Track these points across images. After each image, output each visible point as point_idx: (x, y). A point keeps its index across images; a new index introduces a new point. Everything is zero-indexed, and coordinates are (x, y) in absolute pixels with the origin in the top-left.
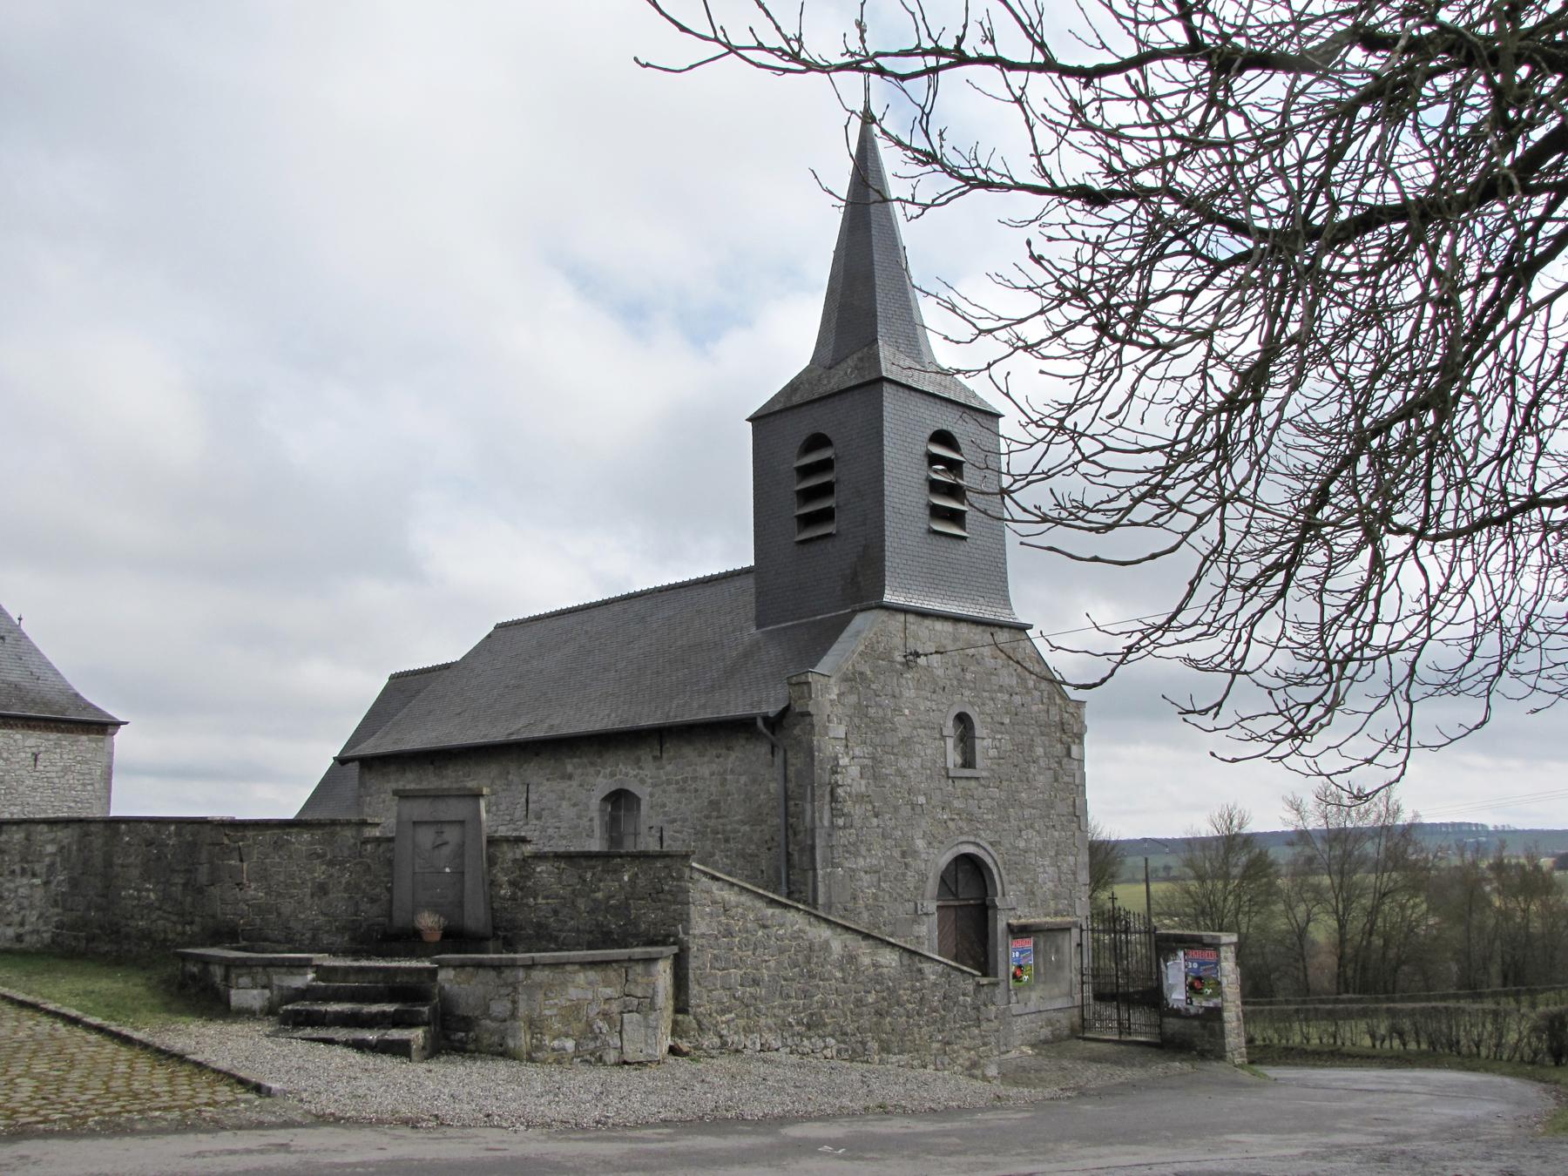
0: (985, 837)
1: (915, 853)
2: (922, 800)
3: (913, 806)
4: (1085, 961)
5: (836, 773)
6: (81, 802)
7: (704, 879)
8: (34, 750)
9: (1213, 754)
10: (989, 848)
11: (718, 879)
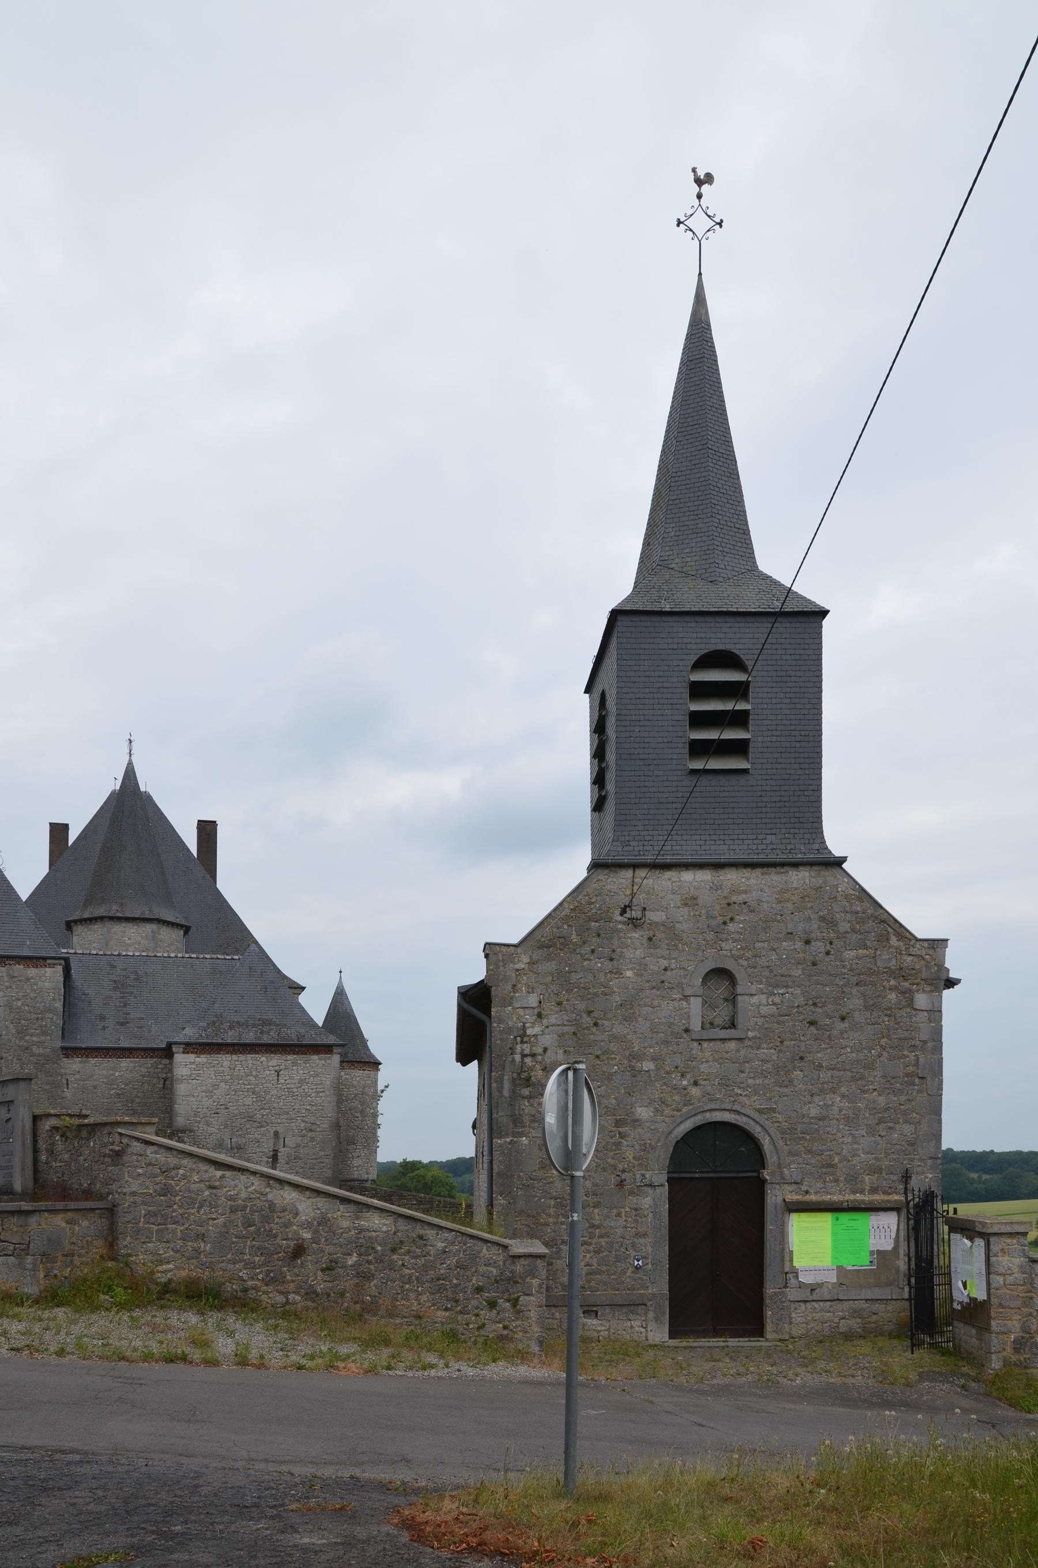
1: (636, 1122)
2: (648, 1065)
3: (635, 1073)
7: (136, 1143)
8: (277, 1068)
9: (341, 972)
10: (756, 1116)
11: (152, 1144)
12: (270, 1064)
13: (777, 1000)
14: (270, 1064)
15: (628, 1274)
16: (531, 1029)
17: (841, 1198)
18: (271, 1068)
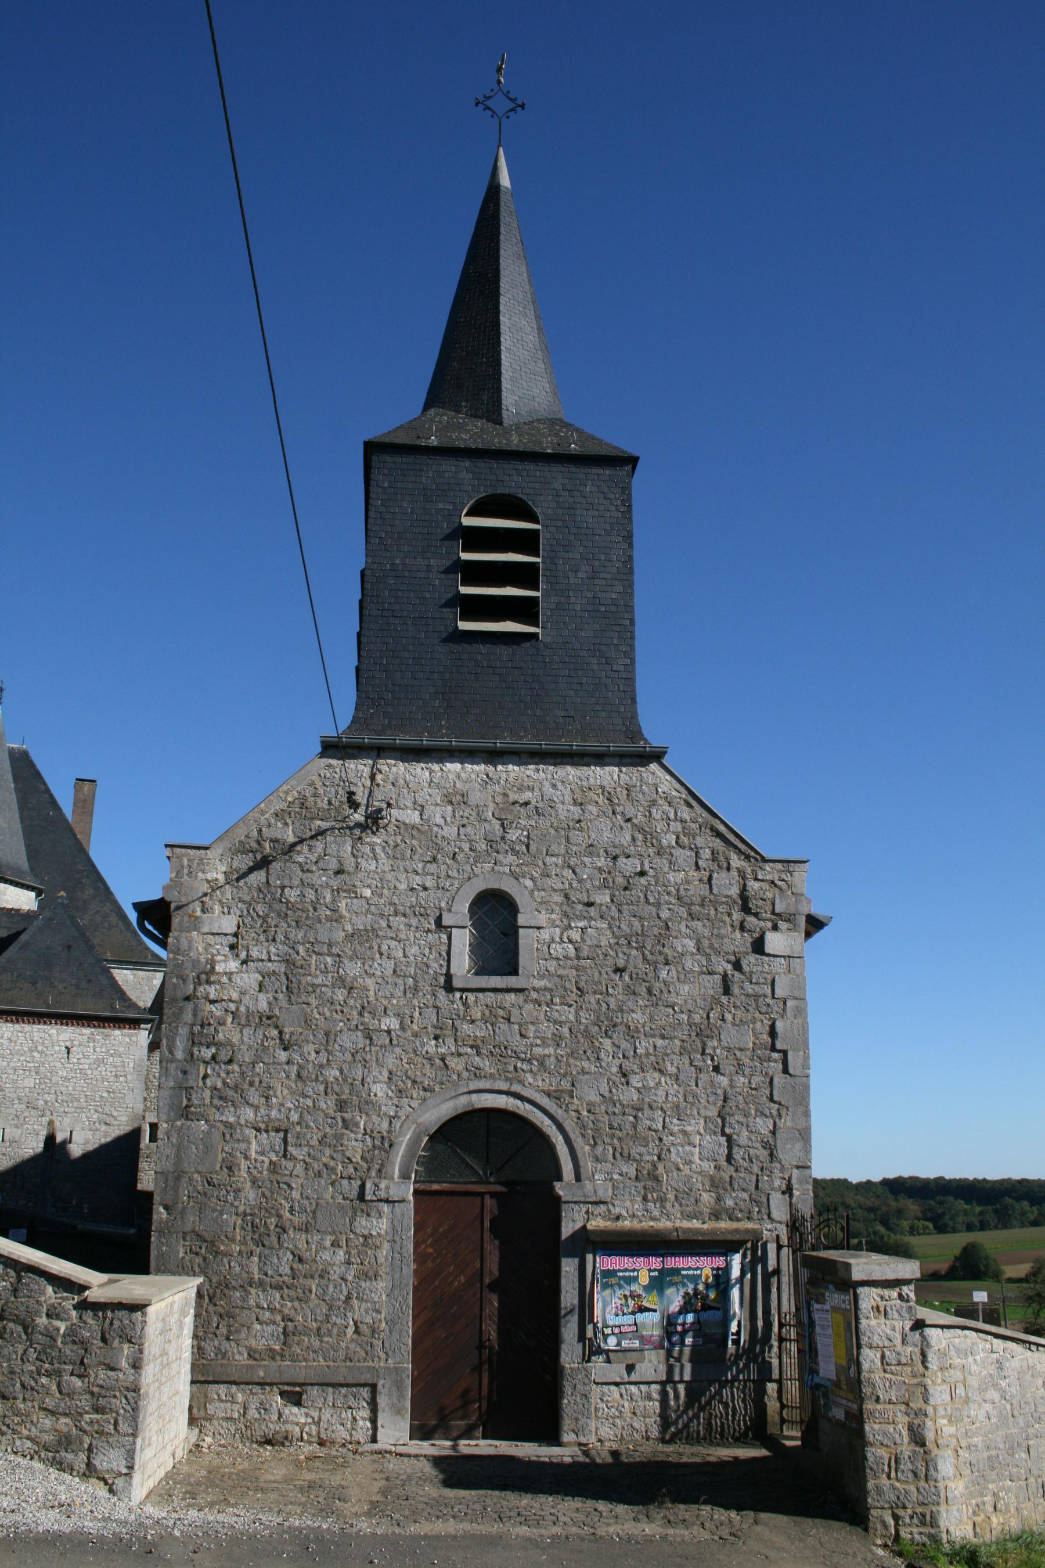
0: (534, 1084)
1: (367, 1105)
4: (775, 1286)
5: (208, 982)
6: (113, 1092)
8: (68, 1044)
10: (545, 1102)
12: (61, 1038)
13: (576, 936)
14: (61, 1038)
15: (349, 1336)
16: (223, 965)
17: (669, 1224)
18: (62, 1043)
